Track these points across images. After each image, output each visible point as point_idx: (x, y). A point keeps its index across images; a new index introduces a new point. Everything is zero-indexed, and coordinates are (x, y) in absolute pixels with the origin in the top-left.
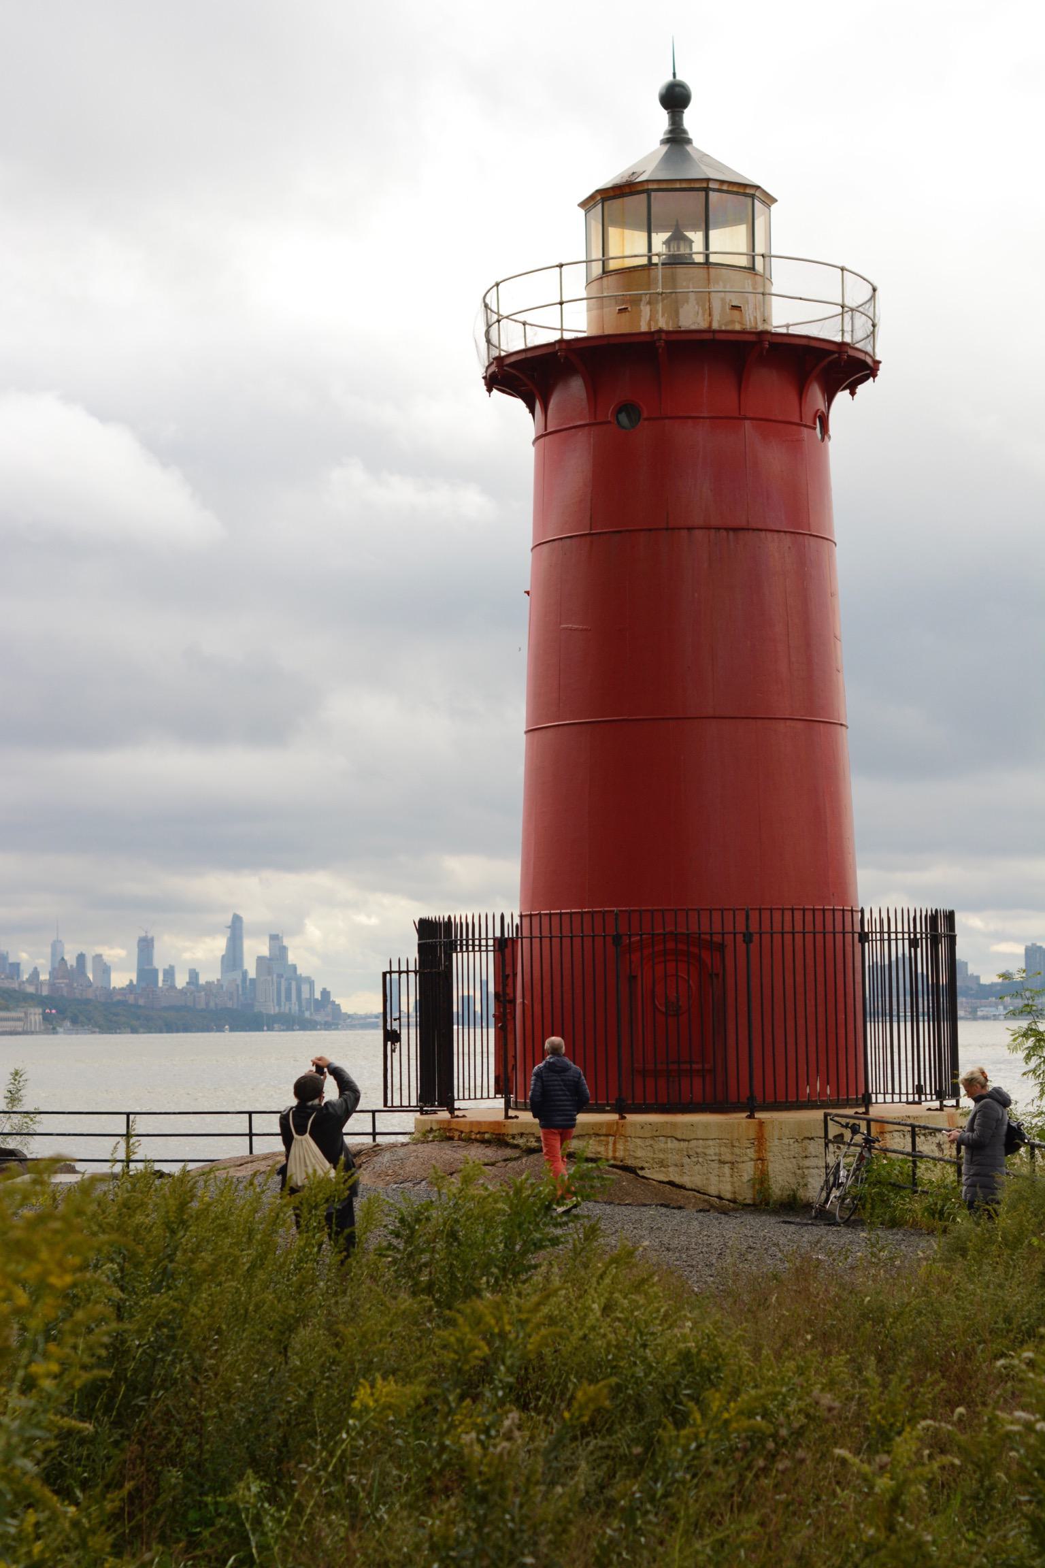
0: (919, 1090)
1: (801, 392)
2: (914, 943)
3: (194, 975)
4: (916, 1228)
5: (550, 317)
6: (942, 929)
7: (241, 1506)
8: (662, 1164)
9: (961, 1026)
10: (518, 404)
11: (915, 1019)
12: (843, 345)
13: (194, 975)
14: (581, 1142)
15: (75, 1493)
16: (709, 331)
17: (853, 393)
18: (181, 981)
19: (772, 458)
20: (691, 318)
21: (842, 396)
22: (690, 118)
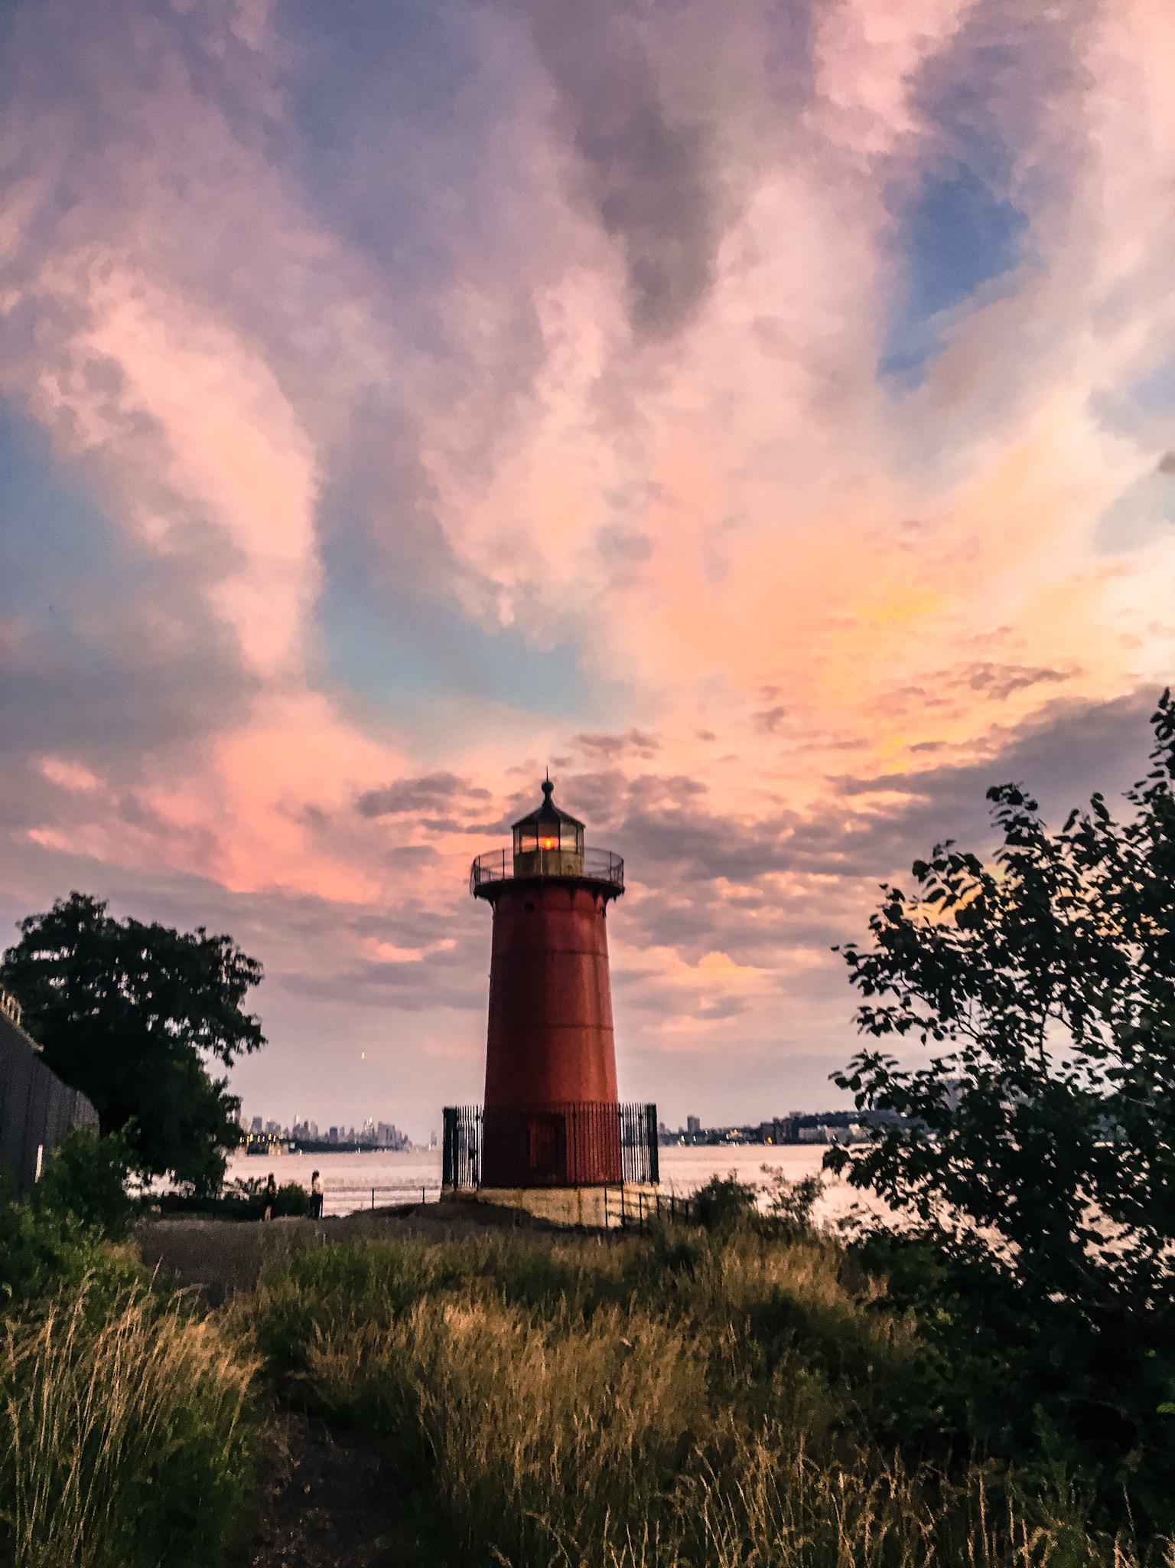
0: (644, 1178)
1: (595, 898)
2: (641, 1117)
3: (352, 1130)
4: (1078, 1035)
5: (500, 870)
6: (651, 1111)
7: (1062, 1080)
8: (540, 1210)
9: (659, 1149)
10: (487, 903)
11: (641, 1145)
12: (611, 882)
13: (352, 1130)
14: (750, 973)
15: (37, 844)
16: (561, 877)
17: (615, 899)
18: (347, 1132)
19: (585, 926)
20: (552, 871)
21: (611, 902)
22: (553, 795)
